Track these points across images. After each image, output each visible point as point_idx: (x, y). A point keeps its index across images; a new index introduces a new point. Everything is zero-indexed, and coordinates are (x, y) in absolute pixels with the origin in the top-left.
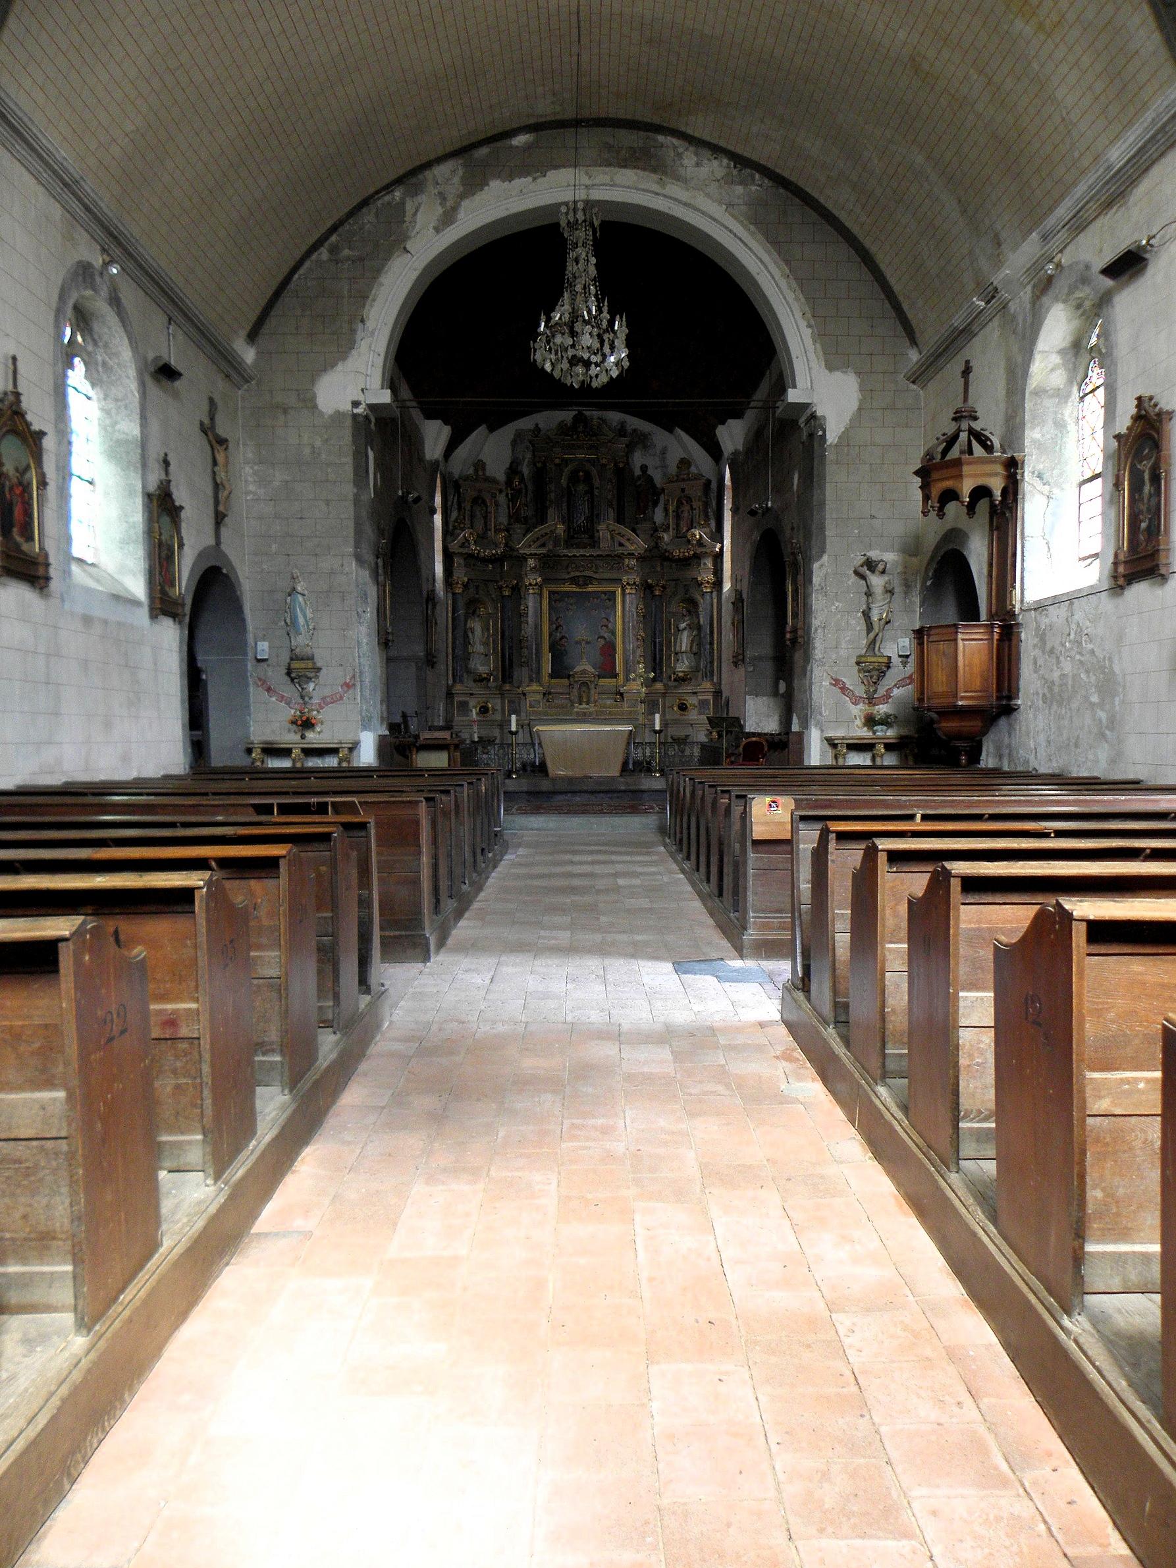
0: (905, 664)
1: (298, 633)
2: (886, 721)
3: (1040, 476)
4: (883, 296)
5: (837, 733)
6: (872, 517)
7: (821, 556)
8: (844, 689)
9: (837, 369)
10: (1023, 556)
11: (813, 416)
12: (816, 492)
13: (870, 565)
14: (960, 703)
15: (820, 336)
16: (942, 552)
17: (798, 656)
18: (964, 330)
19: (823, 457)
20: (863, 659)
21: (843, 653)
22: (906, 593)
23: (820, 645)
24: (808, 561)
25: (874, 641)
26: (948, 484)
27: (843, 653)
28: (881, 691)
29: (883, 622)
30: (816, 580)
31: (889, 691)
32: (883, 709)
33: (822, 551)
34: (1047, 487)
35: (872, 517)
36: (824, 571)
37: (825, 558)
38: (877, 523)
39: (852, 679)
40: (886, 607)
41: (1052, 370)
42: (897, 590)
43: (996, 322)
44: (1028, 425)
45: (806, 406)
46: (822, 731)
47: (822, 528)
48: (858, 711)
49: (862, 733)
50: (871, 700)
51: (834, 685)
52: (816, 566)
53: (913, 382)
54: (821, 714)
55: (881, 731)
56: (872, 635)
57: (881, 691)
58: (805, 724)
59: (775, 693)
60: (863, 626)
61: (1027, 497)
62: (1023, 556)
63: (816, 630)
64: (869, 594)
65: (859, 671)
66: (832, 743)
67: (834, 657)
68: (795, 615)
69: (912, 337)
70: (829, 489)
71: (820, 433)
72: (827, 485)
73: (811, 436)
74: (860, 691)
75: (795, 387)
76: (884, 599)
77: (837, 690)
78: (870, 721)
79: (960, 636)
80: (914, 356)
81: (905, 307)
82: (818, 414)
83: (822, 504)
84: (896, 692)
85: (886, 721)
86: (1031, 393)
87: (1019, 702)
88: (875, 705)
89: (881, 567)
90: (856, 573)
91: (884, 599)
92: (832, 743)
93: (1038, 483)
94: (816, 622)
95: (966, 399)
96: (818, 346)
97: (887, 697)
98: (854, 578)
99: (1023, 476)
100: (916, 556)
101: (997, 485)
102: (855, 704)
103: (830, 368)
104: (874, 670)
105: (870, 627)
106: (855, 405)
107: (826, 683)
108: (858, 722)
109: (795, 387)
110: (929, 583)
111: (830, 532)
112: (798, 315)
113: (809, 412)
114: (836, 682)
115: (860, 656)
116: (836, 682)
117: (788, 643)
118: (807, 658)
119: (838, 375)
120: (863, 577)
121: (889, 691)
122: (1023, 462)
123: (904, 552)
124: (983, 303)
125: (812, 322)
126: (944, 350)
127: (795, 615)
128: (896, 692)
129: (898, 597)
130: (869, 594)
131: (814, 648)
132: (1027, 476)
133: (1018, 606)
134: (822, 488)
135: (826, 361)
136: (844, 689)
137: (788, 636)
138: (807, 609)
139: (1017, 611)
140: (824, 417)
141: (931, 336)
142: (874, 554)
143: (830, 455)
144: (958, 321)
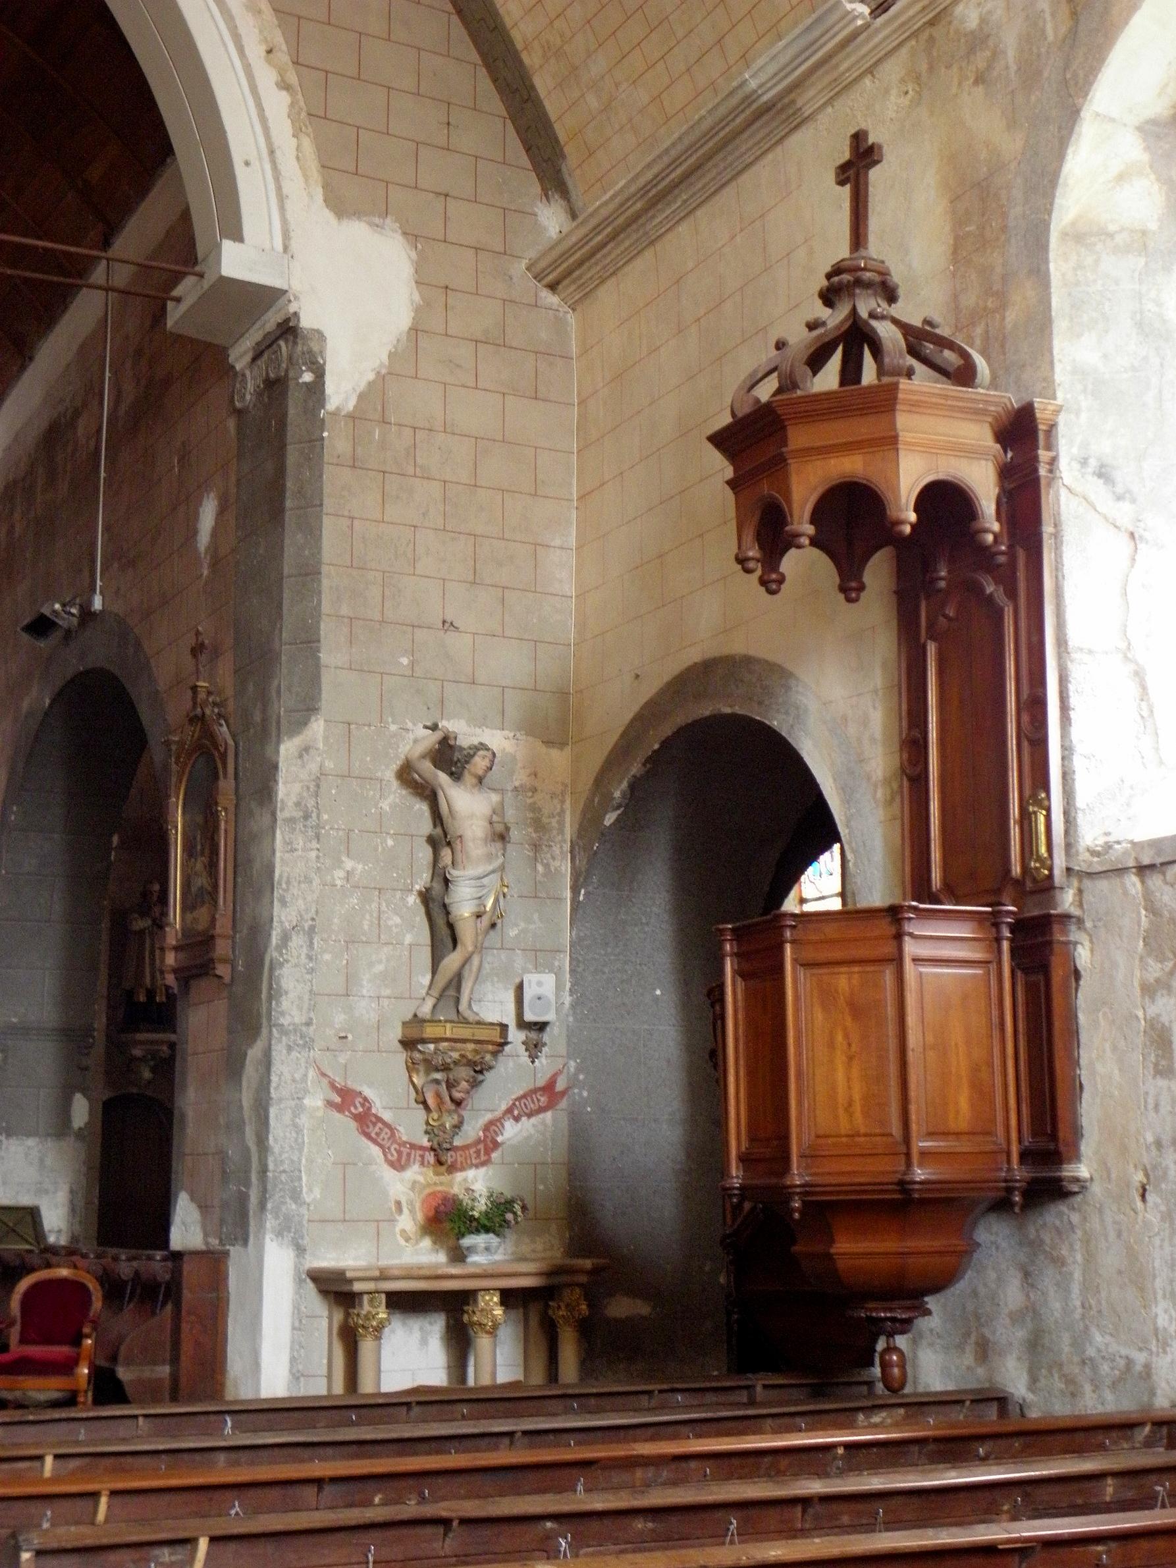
0: (534, 1049)
1: (867, 1417)
2: (495, 1220)
3: (1103, 474)
4: (475, 56)
5: (351, 1257)
6: (448, 625)
7: (305, 723)
8: (366, 1120)
9: (357, 214)
10: (1065, 708)
11: (288, 329)
12: (292, 540)
13: (449, 757)
14: (920, 1174)
15: (315, 116)
16: (680, 719)
17: (202, 1022)
18: (768, 108)
19: (315, 443)
20: (430, 1031)
21: (365, 1010)
22: (536, 847)
23: (297, 986)
24: (262, 734)
25: (456, 981)
26: (851, 466)
27: (365, 1010)
28: (472, 1130)
29: (485, 921)
30: (287, 790)
31: (492, 1126)
32: (477, 1184)
33: (309, 708)
34: (1126, 506)
35: (448, 625)
36: (313, 767)
37: (317, 727)
38: (459, 644)
39: (389, 1088)
40: (493, 881)
41: (1121, 178)
42: (514, 834)
43: (893, 70)
44: (1060, 326)
45: (266, 296)
46: (300, 1250)
47: (310, 642)
48: (406, 1187)
49: (419, 1257)
50: (442, 1155)
51: (340, 1108)
52: (287, 749)
53: (552, 287)
54: (296, 1196)
55: (488, 1254)
56: (452, 961)
57: (472, 1130)
58: (236, 1221)
59: (61, 1127)
60: (418, 933)
61: (1070, 534)
62: (1065, 708)
63: (285, 938)
64: (442, 838)
65: (411, 1067)
66: (336, 1290)
67: (340, 1019)
68: (201, 897)
69: (552, 176)
70: (331, 529)
71: (307, 377)
72: (327, 522)
73: (275, 387)
74: (412, 1126)
75: (238, 237)
76: (490, 857)
77: (345, 1123)
78: (448, 1221)
79: (911, 948)
80: (552, 220)
81: (543, 83)
82: (306, 322)
83: (311, 573)
84: (511, 1131)
85: (495, 1220)
86: (1065, 235)
87: (1083, 1170)
88: (452, 1169)
89: (479, 763)
90: (407, 775)
91: (490, 857)
92: (336, 1290)
93: (1096, 489)
94: (283, 917)
95: (858, 237)
96: (307, 144)
97: (488, 1144)
98: (395, 796)
99: (1053, 461)
100: (562, 745)
101: (983, 482)
102: (398, 1165)
103: (340, 206)
104: (447, 1060)
105: (444, 932)
106: (402, 319)
107: (315, 1101)
108: (407, 1222)
109: (238, 237)
110: (610, 819)
111: (333, 654)
112: (255, 51)
113: (271, 320)
114: (344, 1098)
115: (417, 1021)
116: (344, 1098)
117: (170, 979)
118: (248, 1018)
119: (357, 230)
120: (429, 794)
121: (492, 1126)
122: (1052, 427)
123: (530, 732)
124: (864, 10)
125: (292, 78)
126: (686, 176)
127: (201, 897)
128: (511, 1131)
129: (517, 851)
130: (442, 838)
131: (275, 994)
132: (1067, 469)
133: (1059, 862)
134: (313, 532)
135: (326, 186)
136: (366, 1120)
137: (170, 959)
138: (256, 881)
139: (1058, 873)
140: (320, 336)
141: (611, 166)
142: (466, 733)
143: (336, 442)
144: (760, 77)
